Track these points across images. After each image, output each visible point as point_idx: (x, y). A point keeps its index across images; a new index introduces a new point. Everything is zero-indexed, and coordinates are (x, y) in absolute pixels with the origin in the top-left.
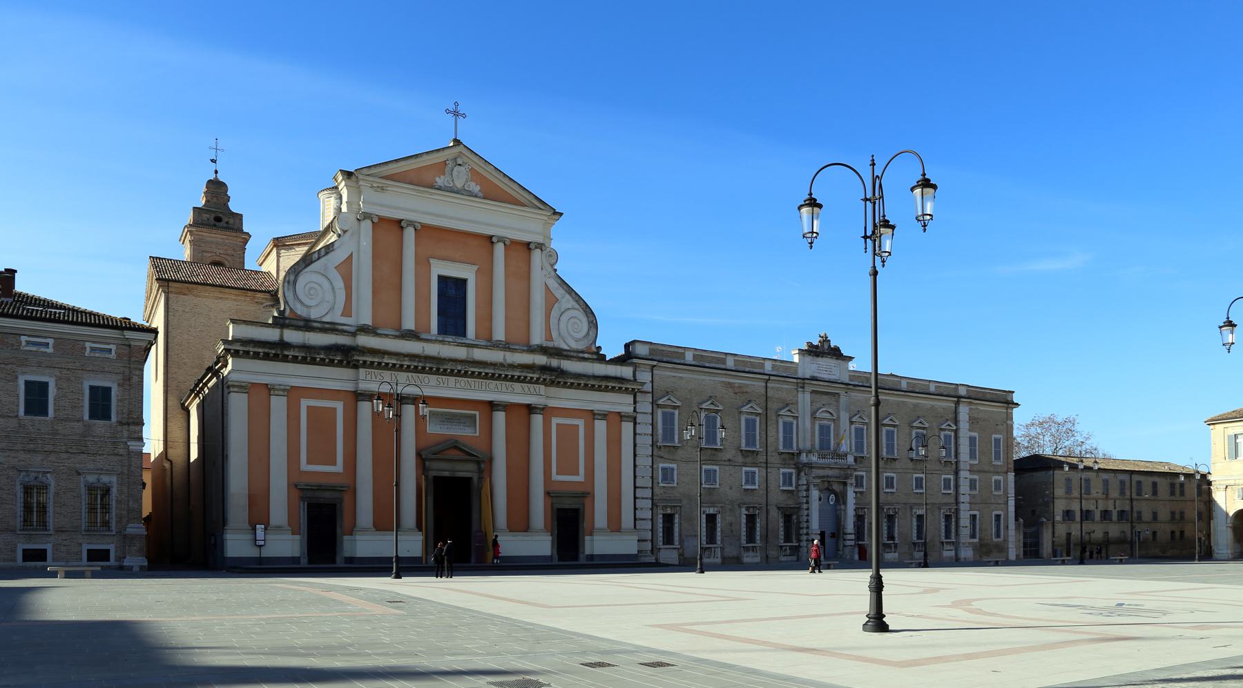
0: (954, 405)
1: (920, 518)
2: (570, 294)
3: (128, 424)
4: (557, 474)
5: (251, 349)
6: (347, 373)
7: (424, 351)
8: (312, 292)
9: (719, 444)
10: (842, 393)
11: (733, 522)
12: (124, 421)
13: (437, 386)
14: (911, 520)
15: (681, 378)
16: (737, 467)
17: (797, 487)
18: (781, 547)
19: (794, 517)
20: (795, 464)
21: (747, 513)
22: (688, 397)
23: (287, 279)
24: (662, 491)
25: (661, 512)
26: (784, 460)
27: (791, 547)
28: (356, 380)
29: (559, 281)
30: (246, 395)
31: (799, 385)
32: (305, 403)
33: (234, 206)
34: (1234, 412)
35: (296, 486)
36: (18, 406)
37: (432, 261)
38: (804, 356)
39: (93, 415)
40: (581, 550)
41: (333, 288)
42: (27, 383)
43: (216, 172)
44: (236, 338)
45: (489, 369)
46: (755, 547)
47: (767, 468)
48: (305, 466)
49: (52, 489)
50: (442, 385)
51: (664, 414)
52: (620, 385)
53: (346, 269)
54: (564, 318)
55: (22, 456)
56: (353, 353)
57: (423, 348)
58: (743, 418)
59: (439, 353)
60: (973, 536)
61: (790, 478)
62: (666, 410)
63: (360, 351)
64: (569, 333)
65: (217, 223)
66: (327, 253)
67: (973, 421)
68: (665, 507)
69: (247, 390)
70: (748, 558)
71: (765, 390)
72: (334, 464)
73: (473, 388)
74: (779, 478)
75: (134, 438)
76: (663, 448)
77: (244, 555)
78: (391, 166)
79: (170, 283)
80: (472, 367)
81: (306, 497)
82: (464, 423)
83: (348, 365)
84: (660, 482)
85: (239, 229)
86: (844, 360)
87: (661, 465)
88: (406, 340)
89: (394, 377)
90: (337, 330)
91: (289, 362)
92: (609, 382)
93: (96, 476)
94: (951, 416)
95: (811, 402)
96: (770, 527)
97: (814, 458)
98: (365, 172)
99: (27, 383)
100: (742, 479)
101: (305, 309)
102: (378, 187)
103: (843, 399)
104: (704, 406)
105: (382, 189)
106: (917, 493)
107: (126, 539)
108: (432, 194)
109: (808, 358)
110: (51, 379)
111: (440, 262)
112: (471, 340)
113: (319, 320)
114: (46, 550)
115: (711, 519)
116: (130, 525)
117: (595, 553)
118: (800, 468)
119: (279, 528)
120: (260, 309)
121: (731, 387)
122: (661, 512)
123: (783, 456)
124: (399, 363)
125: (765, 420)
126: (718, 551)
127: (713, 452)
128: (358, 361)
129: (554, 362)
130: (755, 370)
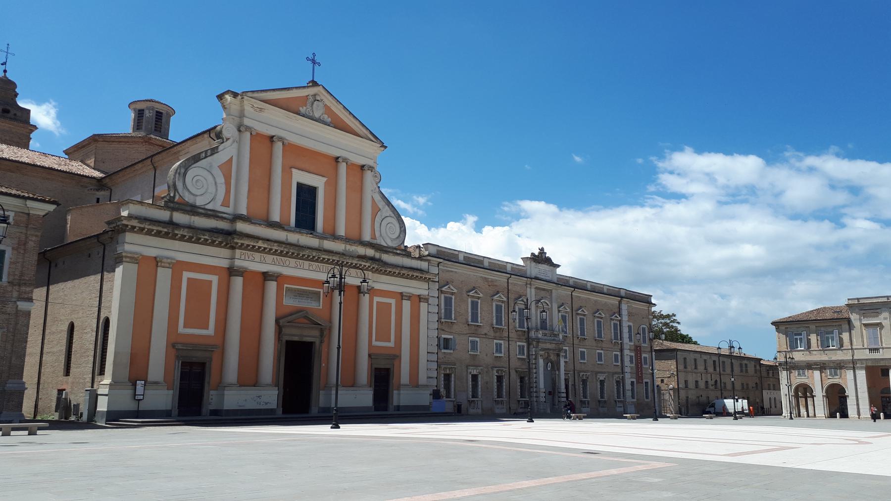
0: (618, 303)
1: (602, 382)
5: (146, 226)
6: (226, 252)
9: (504, 325)
14: (597, 383)
15: (456, 272)
18: (519, 401)
21: (496, 374)
23: (178, 171)
25: (443, 372)
30: (137, 265)
32: (186, 275)
34: (790, 317)
41: (216, 183)
43: (5, 71)
47: (509, 341)
48: (181, 329)
51: (446, 298)
52: (421, 275)
56: (235, 236)
60: (633, 397)
66: (212, 154)
67: (630, 315)
71: (507, 284)
72: (207, 328)
73: (321, 270)
75: (23, 298)
80: (324, 255)
81: (181, 357)
82: (311, 298)
88: (275, 229)
90: (218, 217)
91: (176, 240)
94: (617, 310)
98: (250, 94)
101: (192, 197)
104: (471, 294)
106: (599, 364)
113: (202, 207)
115: (475, 378)
116: (10, 381)
122: (443, 372)
124: (269, 247)
125: (507, 306)
126: (480, 403)
128: (237, 243)
130: (501, 270)
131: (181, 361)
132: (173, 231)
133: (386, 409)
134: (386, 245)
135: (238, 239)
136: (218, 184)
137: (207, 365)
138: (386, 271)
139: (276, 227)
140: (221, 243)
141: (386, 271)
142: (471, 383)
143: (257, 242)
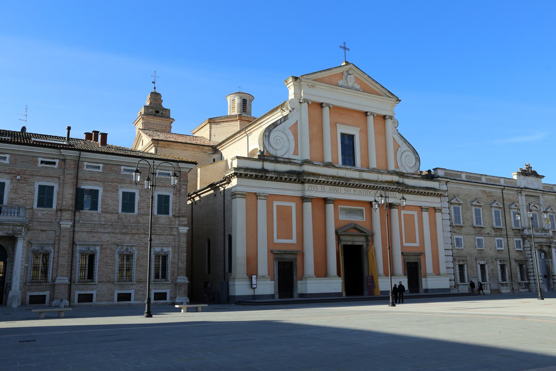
2: (405, 143)
3: (179, 217)
4: (406, 242)
6: (298, 186)
7: (338, 174)
8: (278, 141)
10: (541, 195)
11: (494, 269)
12: (176, 215)
13: (345, 193)
15: (461, 188)
16: (492, 237)
17: (523, 249)
18: (520, 283)
19: (524, 266)
20: (521, 236)
21: (500, 263)
22: (465, 198)
23: (265, 134)
24: (457, 251)
25: (457, 263)
26: (515, 233)
27: (525, 284)
28: (303, 190)
29: (400, 136)
31: (519, 191)
32: (276, 203)
33: (165, 105)
35: (272, 251)
36: (118, 207)
37: (338, 125)
38: (519, 176)
39: (159, 212)
40: (420, 286)
41: (288, 140)
42: (124, 193)
43: (155, 88)
44: (240, 167)
45: (372, 184)
46: (507, 283)
48: (276, 240)
49: (135, 257)
50: (347, 193)
51: (454, 208)
52: (435, 192)
53: (295, 129)
54: (404, 156)
55: (119, 236)
57: (337, 172)
58: (493, 210)
59: (345, 175)
61: (520, 244)
62: (455, 206)
63: (306, 174)
64: (406, 164)
65: (157, 114)
66: (285, 121)
68: (459, 261)
69: (245, 197)
70: (505, 290)
71: (502, 194)
72: (292, 238)
73: (363, 194)
74: (514, 243)
75: (182, 225)
76: (456, 227)
77: (248, 294)
78: (318, 74)
79: (159, 141)
80: (364, 182)
81: (277, 258)
82: (358, 214)
83: (298, 182)
84: (455, 246)
85: (169, 117)
86: (540, 178)
87: (455, 237)
88: (329, 168)
89: (323, 189)
90: (292, 162)
92: (430, 190)
93: (160, 248)
95: (526, 201)
96: (512, 272)
97: (531, 232)
98: (305, 77)
99: (124, 193)
100: (495, 244)
101: (275, 151)
102: (311, 85)
103: (541, 199)
105: (313, 86)
107: (176, 285)
108: (337, 89)
109: (522, 177)
110: (137, 190)
111: (342, 126)
112: (359, 168)
113: (281, 157)
114: (155, 293)
115: (483, 267)
116: (179, 277)
117: (429, 288)
118: (524, 238)
119: (263, 277)
120: (205, 156)
121: (485, 193)
123: (515, 231)
124: (327, 180)
125: (503, 211)
126: (488, 286)
127: (480, 229)
128: (306, 179)
129: (401, 180)
131: (277, 262)
134: (406, 172)
137: (294, 263)
139: (330, 166)
143: (319, 178)
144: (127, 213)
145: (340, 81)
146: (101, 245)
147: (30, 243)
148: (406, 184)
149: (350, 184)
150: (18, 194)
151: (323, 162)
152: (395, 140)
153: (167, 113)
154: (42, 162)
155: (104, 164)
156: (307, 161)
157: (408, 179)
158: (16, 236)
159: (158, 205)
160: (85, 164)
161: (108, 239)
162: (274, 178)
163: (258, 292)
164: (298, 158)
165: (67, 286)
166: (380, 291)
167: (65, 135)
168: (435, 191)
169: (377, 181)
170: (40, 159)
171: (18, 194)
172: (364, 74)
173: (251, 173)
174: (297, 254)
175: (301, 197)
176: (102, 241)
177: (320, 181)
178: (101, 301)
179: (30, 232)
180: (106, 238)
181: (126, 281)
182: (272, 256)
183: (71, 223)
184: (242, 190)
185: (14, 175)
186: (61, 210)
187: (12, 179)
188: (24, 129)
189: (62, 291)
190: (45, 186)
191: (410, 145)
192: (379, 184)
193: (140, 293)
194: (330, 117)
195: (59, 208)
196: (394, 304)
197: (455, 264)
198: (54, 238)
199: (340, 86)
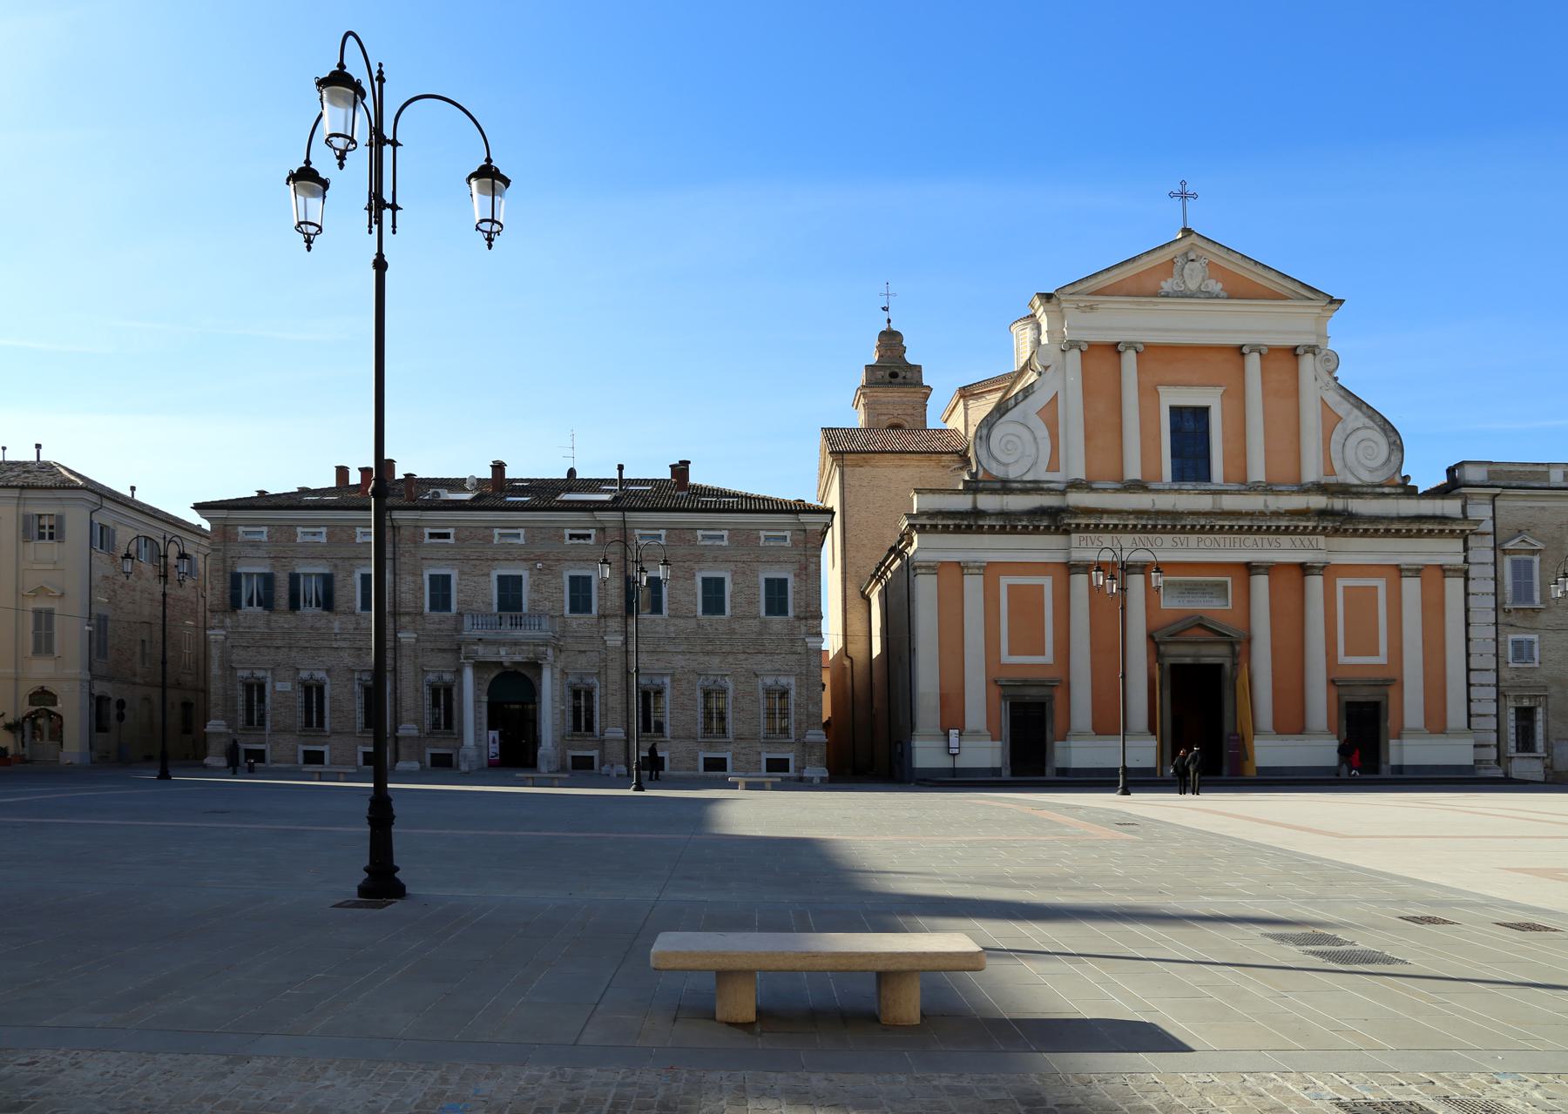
2: (1359, 408)
3: (806, 619)
5: (939, 522)
6: (1056, 540)
8: (1009, 447)
12: (802, 615)
13: (1174, 549)
15: (1543, 508)
23: (979, 434)
24: (1514, 674)
25: (1514, 704)
28: (1068, 549)
29: (1342, 393)
32: (1005, 581)
33: (910, 358)
37: (1161, 389)
40: (1383, 758)
41: (1035, 439)
42: (705, 580)
43: (889, 321)
48: (1006, 658)
50: (1179, 546)
51: (1515, 564)
52: (1441, 527)
53: (1050, 414)
54: (1352, 441)
55: (702, 658)
56: (1064, 515)
57: (1153, 500)
65: (892, 380)
66: (1026, 397)
75: (812, 634)
78: (1100, 278)
80: (1220, 520)
81: (1008, 696)
83: (1057, 531)
85: (919, 383)
88: (1130, 493)
90: (1042, 489)
91: (985, 533)
92: (1424, 523)
99: (705, 580)
101: (1002, 468)
105: (1091, 308)
107: (805, 747)
111: (1173, 389)
112: (1217, 484)
113: (1019, 479)
117: (1406, 763)
119: (976, 733)
122: (1514, 704)
124: (1122, 522)
128: (1070, 525)
129: (1338, 504)
131: (1008, 703)
132: (976, 522)
133: (1377, 771)
134: (1356, 482)
135: (1070, 518)
136: (1038, 440)
138: (1357, 530)
139: (1131, 489)
140: (1047, 528)
141: (1357, 530)
142: (1513, 724)
143: (1101, 518)
144: (712, 617)
145: (1166, 281)
146: (673, 675)
147: (564, 673)
148: (1354, 512)
149: (1184, 527)
150: (542, 593)
151: (1121, 479)
152: (1326, 404)
153: (917, 374)
154: (572, 536)
155: (667, 529)
156: (1078, 482)
157: (1361, 498)
158: (540, 662)
159: (767, 599)
160: (637, 532)
161: (683, 663)
162: (998, 527)
163: (961, 763)
164: (1059, 477)
165: (623, 744)
166: (1257, 768)
167: (616, 476)
168: (1440, 524)
169: (1262, 514)
170: (567, 532)
171: (542, 593)
172: (1230, 252)
173: (945, 522)
174: (1053, 686)
175: (1065, 563)
176: (673, 668)
177: (1106, 526)
178: (678, 770)
179: (563, 656)
180: (679, 661)
181: (717, 737)
182: (995, 691)
183: (621, 638)
184: (927, 559)
185: (534, 562)
186: (605, 616)
187: (531, 570)
188: (572, 472)
189: (616, 750)
190: (578, 577)
191: (1371, 413)
192: (1266, 521)
193: (742, 758)
194: (1139, 372)
195: (1468, 496)
196: (1127, 791)
197: (1506, 705)
198: (597, 664)
199: (1162, 294)
